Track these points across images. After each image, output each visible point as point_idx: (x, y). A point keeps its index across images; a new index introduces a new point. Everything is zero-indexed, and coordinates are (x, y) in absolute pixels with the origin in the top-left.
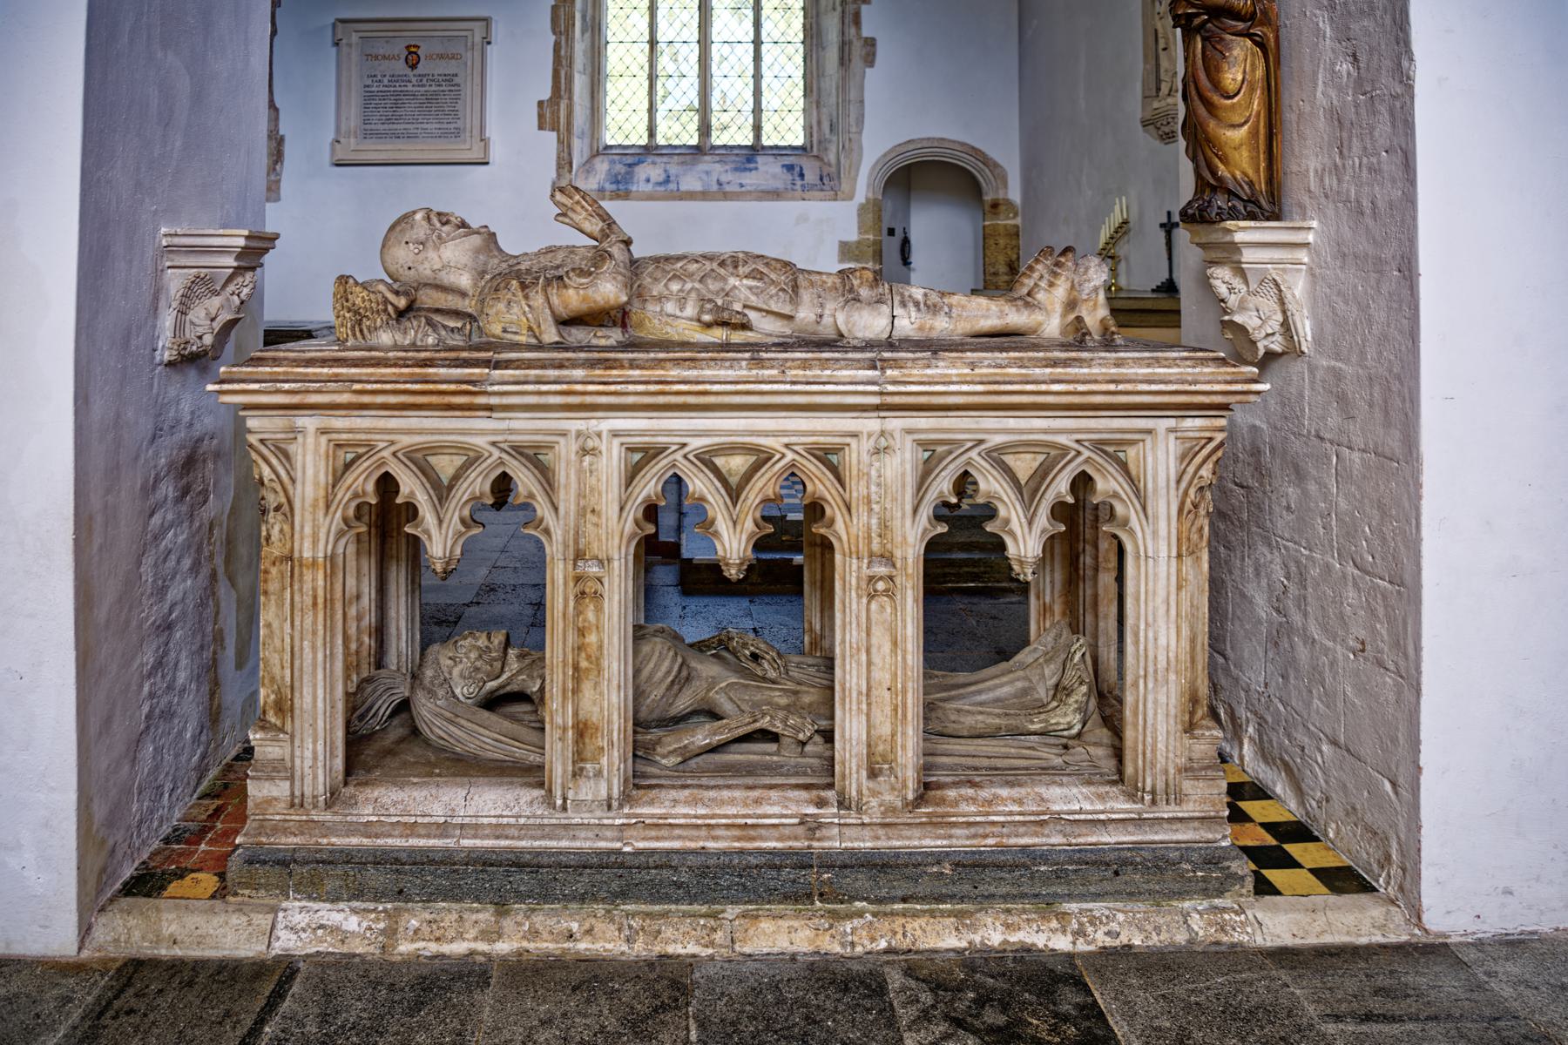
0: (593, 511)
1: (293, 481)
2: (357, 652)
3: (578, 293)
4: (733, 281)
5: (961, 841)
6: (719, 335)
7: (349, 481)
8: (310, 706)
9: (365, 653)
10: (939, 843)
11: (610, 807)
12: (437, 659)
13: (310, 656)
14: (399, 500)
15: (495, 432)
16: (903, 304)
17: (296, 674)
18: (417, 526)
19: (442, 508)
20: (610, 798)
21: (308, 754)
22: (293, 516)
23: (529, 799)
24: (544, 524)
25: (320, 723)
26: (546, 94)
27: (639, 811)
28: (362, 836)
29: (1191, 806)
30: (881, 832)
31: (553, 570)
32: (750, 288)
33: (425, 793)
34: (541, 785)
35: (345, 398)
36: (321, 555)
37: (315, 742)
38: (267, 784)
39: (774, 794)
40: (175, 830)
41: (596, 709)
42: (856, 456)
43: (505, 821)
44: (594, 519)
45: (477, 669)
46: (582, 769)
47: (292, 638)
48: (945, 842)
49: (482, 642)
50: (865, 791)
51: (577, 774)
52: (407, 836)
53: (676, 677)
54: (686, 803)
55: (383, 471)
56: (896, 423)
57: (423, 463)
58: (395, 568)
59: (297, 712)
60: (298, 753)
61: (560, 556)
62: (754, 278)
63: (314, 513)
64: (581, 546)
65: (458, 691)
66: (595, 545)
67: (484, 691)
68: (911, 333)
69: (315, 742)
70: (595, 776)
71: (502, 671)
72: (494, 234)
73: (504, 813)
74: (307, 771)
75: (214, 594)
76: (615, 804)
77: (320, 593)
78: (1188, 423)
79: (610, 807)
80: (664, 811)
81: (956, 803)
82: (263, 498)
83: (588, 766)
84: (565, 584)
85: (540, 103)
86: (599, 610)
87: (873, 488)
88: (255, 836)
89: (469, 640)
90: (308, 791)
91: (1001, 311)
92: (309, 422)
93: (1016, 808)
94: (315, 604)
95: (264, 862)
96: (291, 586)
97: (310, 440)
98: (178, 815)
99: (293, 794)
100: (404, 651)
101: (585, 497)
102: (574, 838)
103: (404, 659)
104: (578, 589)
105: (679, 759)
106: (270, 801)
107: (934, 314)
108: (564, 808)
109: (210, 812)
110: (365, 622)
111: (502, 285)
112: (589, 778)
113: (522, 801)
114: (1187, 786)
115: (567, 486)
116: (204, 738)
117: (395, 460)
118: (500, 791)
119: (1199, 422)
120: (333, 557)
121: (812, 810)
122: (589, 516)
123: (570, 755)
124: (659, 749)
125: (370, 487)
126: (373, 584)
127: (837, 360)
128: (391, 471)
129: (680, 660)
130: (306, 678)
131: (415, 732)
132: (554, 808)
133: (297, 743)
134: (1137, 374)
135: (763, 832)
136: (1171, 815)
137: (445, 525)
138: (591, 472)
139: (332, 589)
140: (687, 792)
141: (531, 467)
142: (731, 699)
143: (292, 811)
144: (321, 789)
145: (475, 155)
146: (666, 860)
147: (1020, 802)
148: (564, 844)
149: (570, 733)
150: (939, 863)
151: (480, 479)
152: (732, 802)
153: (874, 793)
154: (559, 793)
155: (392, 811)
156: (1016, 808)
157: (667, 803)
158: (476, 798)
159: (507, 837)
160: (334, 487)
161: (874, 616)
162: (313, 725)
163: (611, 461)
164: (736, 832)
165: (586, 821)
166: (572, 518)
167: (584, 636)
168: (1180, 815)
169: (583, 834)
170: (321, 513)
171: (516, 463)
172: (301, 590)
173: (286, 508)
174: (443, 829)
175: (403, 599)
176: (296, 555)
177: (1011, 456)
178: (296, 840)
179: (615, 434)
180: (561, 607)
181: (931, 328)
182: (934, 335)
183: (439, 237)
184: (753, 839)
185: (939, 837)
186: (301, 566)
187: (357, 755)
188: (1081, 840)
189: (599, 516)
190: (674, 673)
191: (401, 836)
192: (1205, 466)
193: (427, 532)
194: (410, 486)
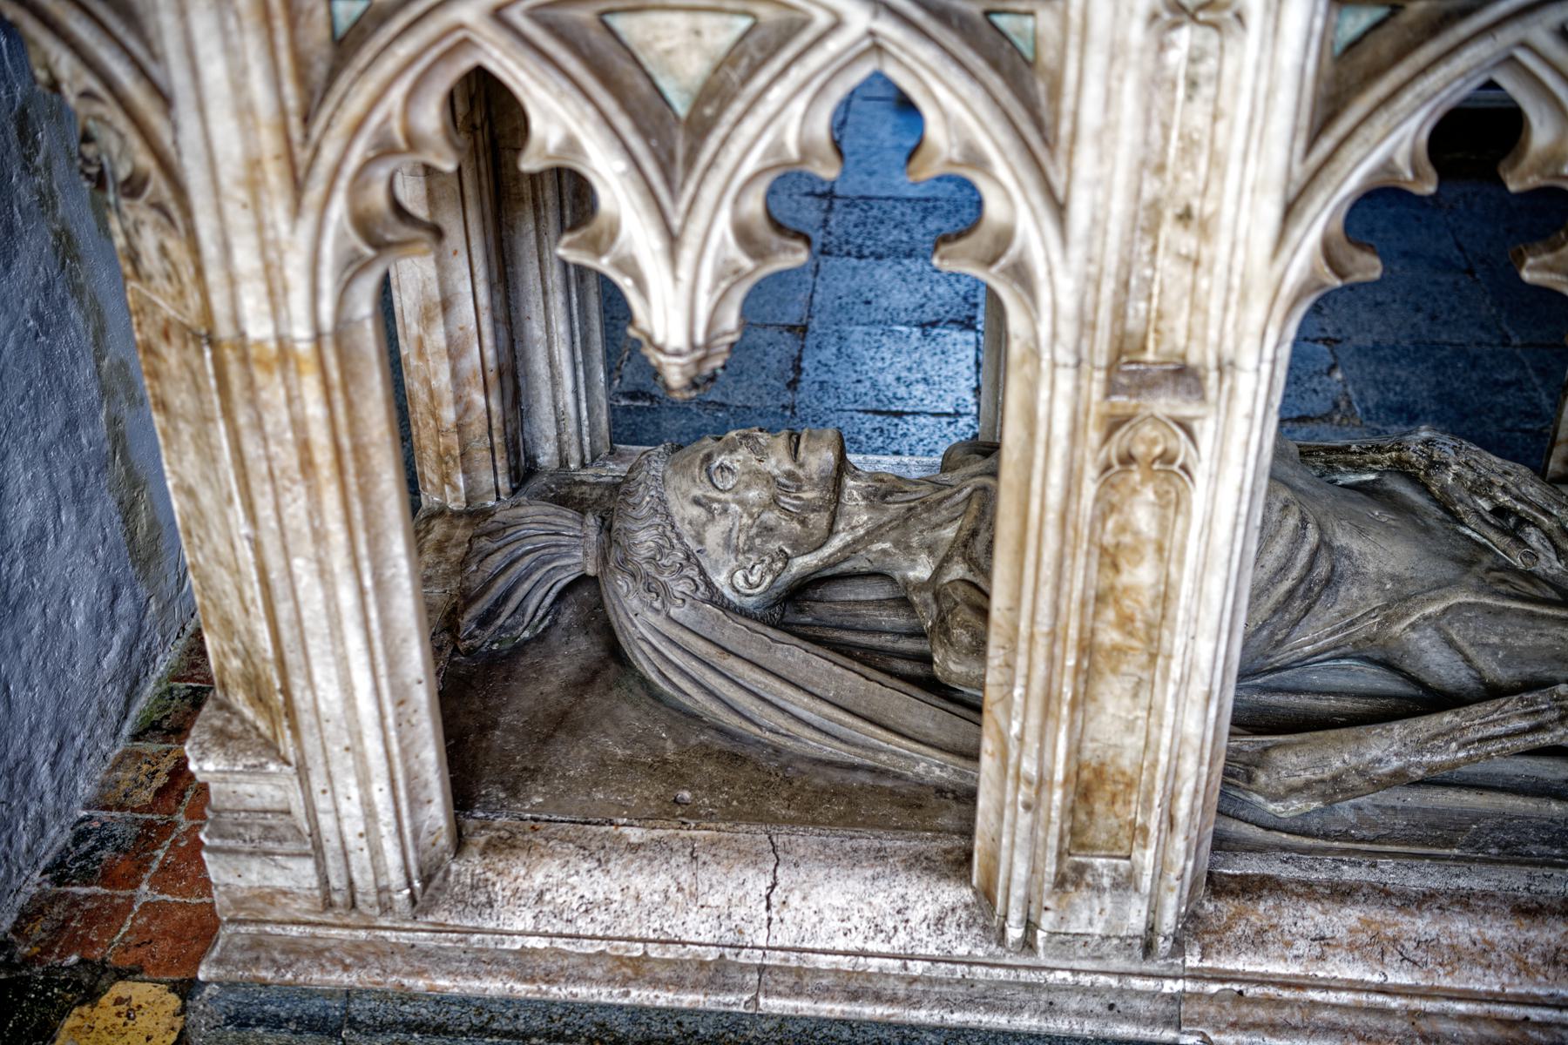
0: (1185, 216)
1: (165, 99)
2: (460, 427)
7: (355, 106)
8: (338, 708)
9: (477, 427)
12: (663, 501)
13: (319, 594)
14: (529, 163)
17: (287, 634)
18: (596, 246)
19: (674, 194)
21: (351, 808)
22: (188, 213)
23: (932, 910)
24: (1012, 253)
25: (373, 746)
28: (511, 975)
31: (1032, 386)
33: (662, 881)
34: (959, 865)
36: (301, 332)
37: (364, 782)
38: (255, 864)
40: (80, 837)
41: (1135, 741)
44: (1187, 242)
45: (767, 531)
46: (1080, 869)
47: (257, 546)
49: (777, 462)
51: (1070, 879)
52: (626, 982)
53: (1301, 580)
55: (465, 63)
57: (596, 37)
58: (530, 225)
59: (306, 719)
60: (323, 803)
61: (1065, 356)
63: (255, 205)
64: (1133, 324)
65: (720, 580)
66: (1180, 323)
67: (786, 577)
69: (364, 782)
70: (1116, 885)
71: (831, 532)
73: (871, 946)
74: (352, 841)
75: (77, 291)
76: (1163, 945)
77: (319, 437)
79: (1148, 948)
80: (1295, 969)
82: (87, 138)
83: (1098, 862)
84: (1074, 433)
86: (1172, 504)
88: (245, 965)
89: (743, 453)
90: (364, 881)
94: (307, 465)
95: (276, 1023)
96: (228, 413)
98: (85, 789)
99: (324, 881)
100: (571, 410)
101: (1161, 169)
103: (571, 428)
104: (1113, 450)
108: (1028, 944)
109: (161, 780)
110: (472, 360)
112: (1099, 890)
113: (915, 916)
115: (1107, 130)
116: (125, 606)
117: (505, 39)
118: (855, 885)
120: (343, 327)
122: (1168, 230)
123: (1053, 841)
124: (1262, 778)
125: (430, 118)
126: (481, 273)
128: (492, 66)
129: (1312, 537)
130: (316, 646)
131: (615, 653)
132: (1001, 940)
133: (317, 783)
137: (687, 255)
138: (1193, 84)
139: (353, 421)
140: (1351, 915)
141: (978, 64)
142: (1450, 643)
143: (329, 917)
144: (395, 877)
149: (1058, 796)
151: (799, 106)
154: (1015, 916)
155: (583, 926)
157: (1302, 946)
158: (795, 900)
160: (307, 119)
162: (355, 749)
165: (1085, 980)
166: (1114, 240)
167: (1115, 567)
170: (278, 211)
171: (927, 53)
172: (258, 425)
173: (158, 185)
175: (557, 301)
176: (224, 330)
180: (1054, 496)
186: (244, 359)
187: (484, 729)
189: (1205, 229)
190: (1295, 573)
191: (610, 981)
193: (629, 266)
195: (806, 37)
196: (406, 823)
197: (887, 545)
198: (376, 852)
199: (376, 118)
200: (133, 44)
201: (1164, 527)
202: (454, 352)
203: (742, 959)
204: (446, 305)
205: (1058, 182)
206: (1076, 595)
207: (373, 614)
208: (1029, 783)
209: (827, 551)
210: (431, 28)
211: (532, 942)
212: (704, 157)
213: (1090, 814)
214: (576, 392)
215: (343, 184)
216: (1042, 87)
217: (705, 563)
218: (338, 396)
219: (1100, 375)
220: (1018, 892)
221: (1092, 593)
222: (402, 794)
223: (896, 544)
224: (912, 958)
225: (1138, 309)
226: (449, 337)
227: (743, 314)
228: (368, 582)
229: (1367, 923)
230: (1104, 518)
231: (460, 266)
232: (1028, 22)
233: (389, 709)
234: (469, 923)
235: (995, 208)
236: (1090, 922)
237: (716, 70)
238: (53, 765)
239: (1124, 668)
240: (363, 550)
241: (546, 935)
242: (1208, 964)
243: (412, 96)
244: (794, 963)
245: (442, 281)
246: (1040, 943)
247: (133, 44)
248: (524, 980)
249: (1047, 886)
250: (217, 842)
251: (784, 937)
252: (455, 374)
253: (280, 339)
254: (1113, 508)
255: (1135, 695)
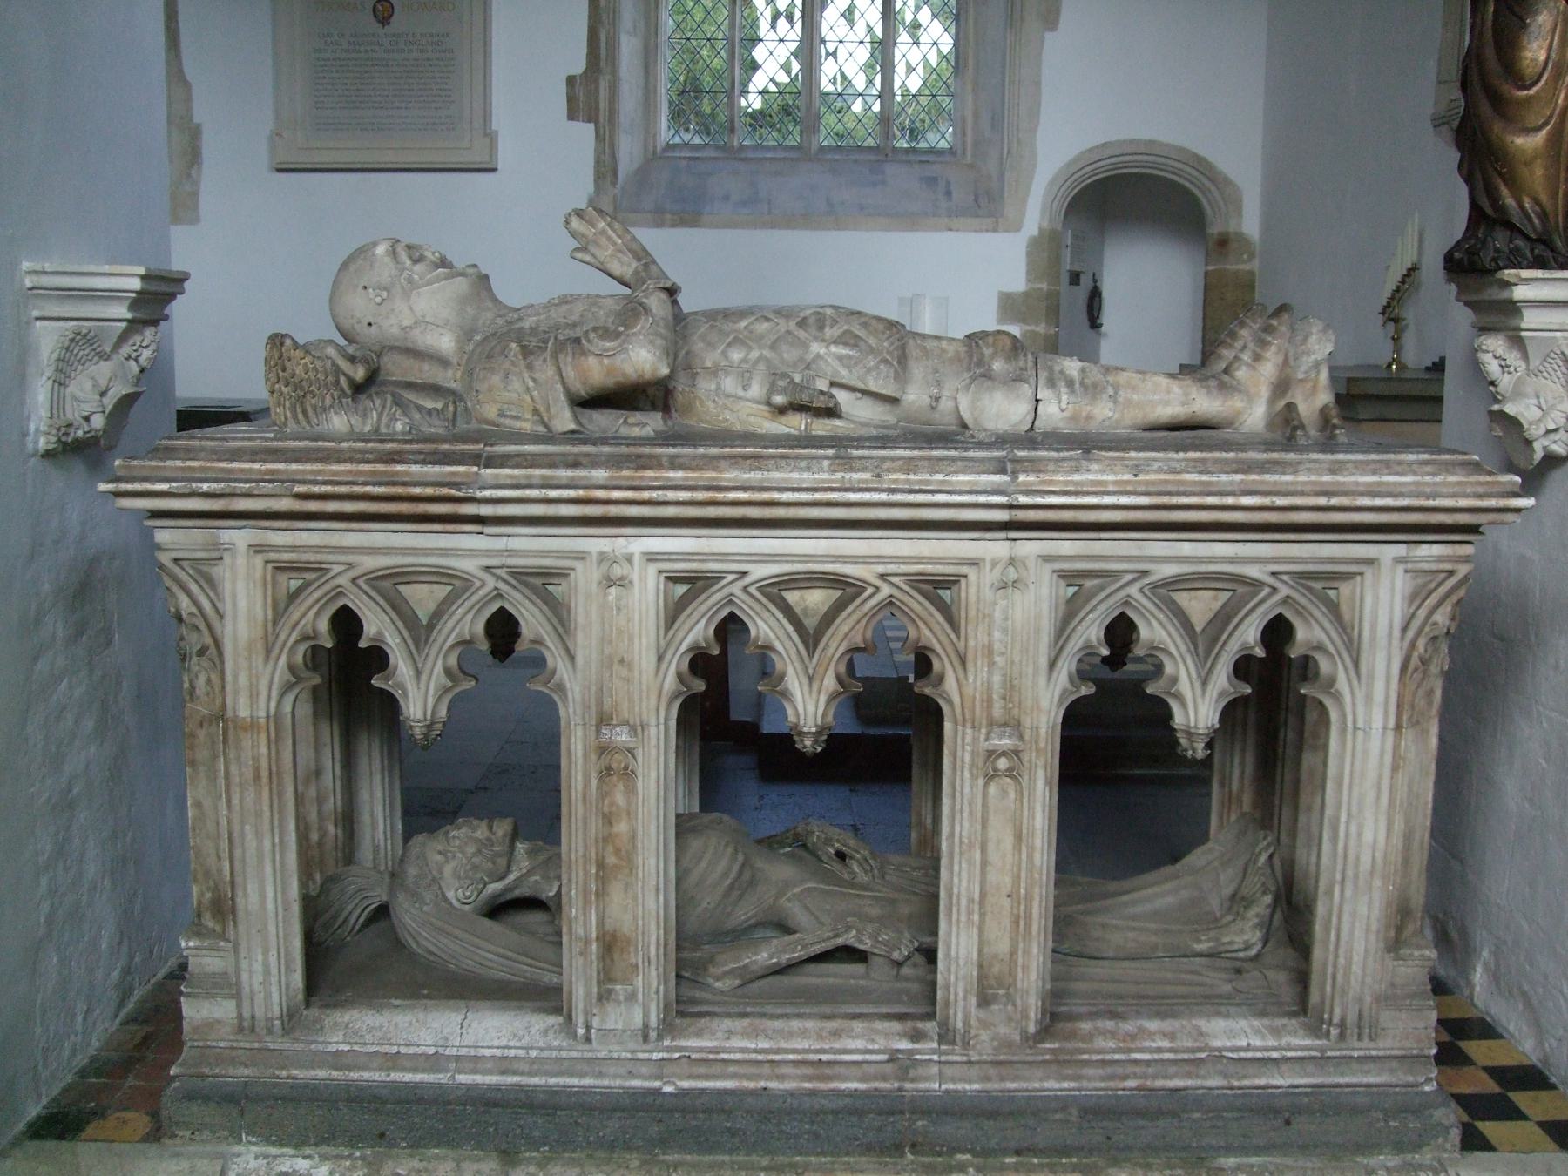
0: (622, 661)
1: (221, 616)
3: (601, 363)
4: (816, 348)
5: (1094, 1085)
6: (796, 423)
7: (295, 617)
10: (1065, 1085)
11: (646, 1038)
15: (488, 553)
16: (1051, 383)
20: (646, 1026)
21: (258, 967)
22: (222, 662)
26: (579, 66)
27: (683, 1043)
29: (1389, 1042)
30: (992, 1071)
32: (840, 358)
34: (557, 1010)
35: (285, 504)
39: (858, 1026)
42: (976, 590)
43: (512, 1053)
44: (624, 672)
46: (610, 992)
48: (1072, 1085)
50: (974, 1022)
51: (604, 997)
53: (735, 880)
54: (745, 1034)
55: (340, 603)
56: (1031, 547)
62: (846, 344)
66: (625, 706)
68: (1061, 425)
69: (266, 952)
70: (626, 1000)
71: (508, 870)
72: (486, 277)
73: (511, 1044)
74: (257, 987)
76: (653, 1035)
77: (264, 763)
78: (1424, 551)
79: (646, 1038)
81: (1089, 1037)
83: (618, 987)
84: (585, 756)
85: (571, 81)
86: (631, 790)
87: (997, 635)
89: (464, 830)
90: (260, 1013)
91: (1186, 395)
92: (239, 537)
93: (1166, 1044)
94: (257, 778)
97: (241, 561)
99: (240, 1017)
101: (610, 642)
102: (601, 1075)
105: (738, 982)
106: (211, 1025)
107: (1094, 398)
108: (588, 1040)
111: (498, 349)
112: (619, 1003)
113: (533, 1031)
114: (1386, 1017)
119: (1436, 550)
120: (278, 717)
121: (905, 1045)
122: (616, 667)
127: (954, 460)
128: (350, 605)
134: (1357, 483)
135: (842, 1070)
136: (1362, 1053)
137: (424, 677)
138: (619, 609)
141: (538, 601)
145: (478, 157)
146: (721, 1103)
147: (1171, 1036)
148: (587, 1082)
149: (594, 946)
150: (1064, 1109)
151: (469, 617)
152: (804, 1034)
153: (985, 1025)
155: (368, 1038)
156: (1166, 1044)
159: (515, 1073)
160: (275, 624)
161: (992, 801)
162: (263, 931)
163: (647, 592)
164: (809, 1071)
167: (610, 824)
168: (1374, 1053)
169: (612, 1070)
171: (518, 595)
173: (212, 651)
174: (434, 1062)
176: (230, 714)
177: (1185, 594)
178: (246, 1072)
179: (651, 558)
180: (580, 787)
181: (1089, 418)
182: (1093, 427)
183: (410, 280)
184: (829, 1078)
185: (1065, 1078)
188: (1246, 1082)
189: (630, 666)
192: (1440, 610)
194: (377, 625)
195: (472, 590)
196: (283, 979)
197: (538, 878)
198: (268, 996)
199: (303, 622)
200: (212, 594)
201: (629, 804)
202: (320, 800)
203: (447, 1053)
204: (318, 773)
205: (571, 648)
206: (593, 836)
207: (278, 857)
208: (580, 939)
209: (507, 881)
210: (327, 587)
211: (341, 1047)
212: (432, 638)
213: (612, 960)
214: (385, 833)
215: (286, 650)
216: (565, 613)
217: (443, 885)
218: (273, 746)
219: (594, 728)
220: (581, 1006)
221: (600, 836)
222: (283, 961)
223: (543, 878)
224: (532, 1048)
225: (607, 702)
226: (318, 791)
227: (449, 709)
228: (277, 841)
229: (750, 1024)
230: (603, 799)
231: (327, 751)
232: (560, 588)
233: (280, 910)
234: (311, 1038)
235: (550, 662)
236: (616, 1023)
237: (439, 605)
238: (85, 1019)
239: (620, 877)
240: (276, 823)
241: (349, 1043)
242: (674, 1043)
243: (318, 614)
244: (473, 1053)
245: (317, 760)
246: (593, 1036)
247: (212, 594)
248: (336, 1069)
249: (594, 1001)
250: (189, 990)
251: (469, 1040)
252: (319, 813)
253: (252, 717)
254: (607, 793)
255: (626, 891)
